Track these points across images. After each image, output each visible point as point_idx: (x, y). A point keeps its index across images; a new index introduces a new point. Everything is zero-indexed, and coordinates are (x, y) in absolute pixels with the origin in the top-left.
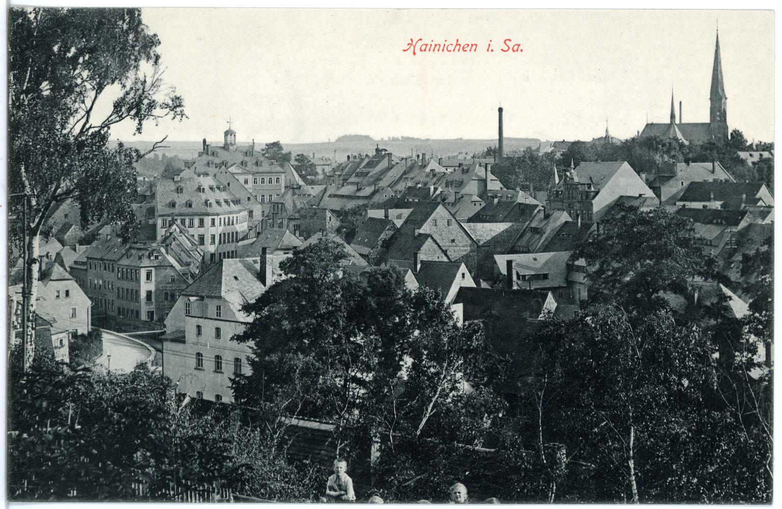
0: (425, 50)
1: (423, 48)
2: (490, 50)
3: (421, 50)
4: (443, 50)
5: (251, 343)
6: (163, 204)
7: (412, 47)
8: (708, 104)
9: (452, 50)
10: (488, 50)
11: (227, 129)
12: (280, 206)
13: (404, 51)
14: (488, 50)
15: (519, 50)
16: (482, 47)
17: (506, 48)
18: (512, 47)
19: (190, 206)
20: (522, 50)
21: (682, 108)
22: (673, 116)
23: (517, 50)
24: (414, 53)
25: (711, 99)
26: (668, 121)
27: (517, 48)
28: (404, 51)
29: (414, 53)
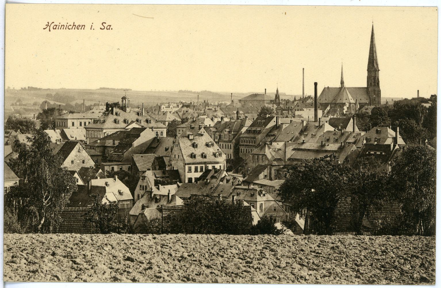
0: (56, 29)
1: (55, 27)
2: (92, 28)
3: (54, 29)
4: (75, 29)
5: (231, 203)
6: (187, 155)
7: (49, 27)
8: (366, 74)
9: (71, 28)
10: (91, 29)
11: (124, 96)
12: (260, 156)
13: (44, 29)
14: (91, 29)
15: (110, 29)
16: (88, 27)
17: (103, 27)
18: (106, 27)
19: (205, 157)
20: (112, 29)
21: (304, 75)
22: (342, 83)
23: (109, 29)
24: (50, 31)
25: (367, 70)
26: (339, 85)
27: (109, 28)
28: (44, 29)
29: (50, 31)
